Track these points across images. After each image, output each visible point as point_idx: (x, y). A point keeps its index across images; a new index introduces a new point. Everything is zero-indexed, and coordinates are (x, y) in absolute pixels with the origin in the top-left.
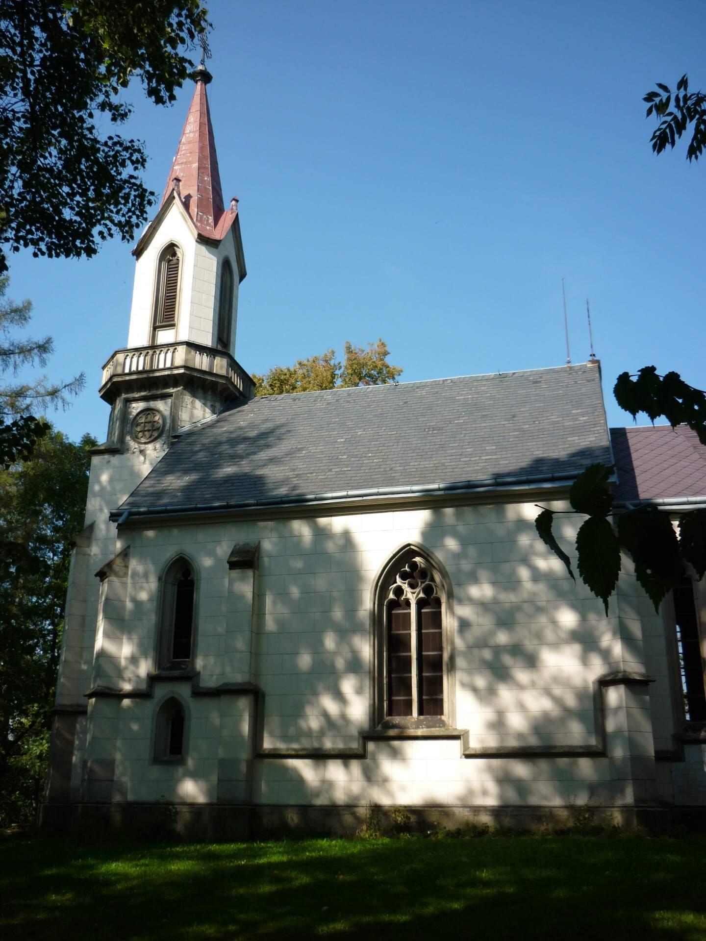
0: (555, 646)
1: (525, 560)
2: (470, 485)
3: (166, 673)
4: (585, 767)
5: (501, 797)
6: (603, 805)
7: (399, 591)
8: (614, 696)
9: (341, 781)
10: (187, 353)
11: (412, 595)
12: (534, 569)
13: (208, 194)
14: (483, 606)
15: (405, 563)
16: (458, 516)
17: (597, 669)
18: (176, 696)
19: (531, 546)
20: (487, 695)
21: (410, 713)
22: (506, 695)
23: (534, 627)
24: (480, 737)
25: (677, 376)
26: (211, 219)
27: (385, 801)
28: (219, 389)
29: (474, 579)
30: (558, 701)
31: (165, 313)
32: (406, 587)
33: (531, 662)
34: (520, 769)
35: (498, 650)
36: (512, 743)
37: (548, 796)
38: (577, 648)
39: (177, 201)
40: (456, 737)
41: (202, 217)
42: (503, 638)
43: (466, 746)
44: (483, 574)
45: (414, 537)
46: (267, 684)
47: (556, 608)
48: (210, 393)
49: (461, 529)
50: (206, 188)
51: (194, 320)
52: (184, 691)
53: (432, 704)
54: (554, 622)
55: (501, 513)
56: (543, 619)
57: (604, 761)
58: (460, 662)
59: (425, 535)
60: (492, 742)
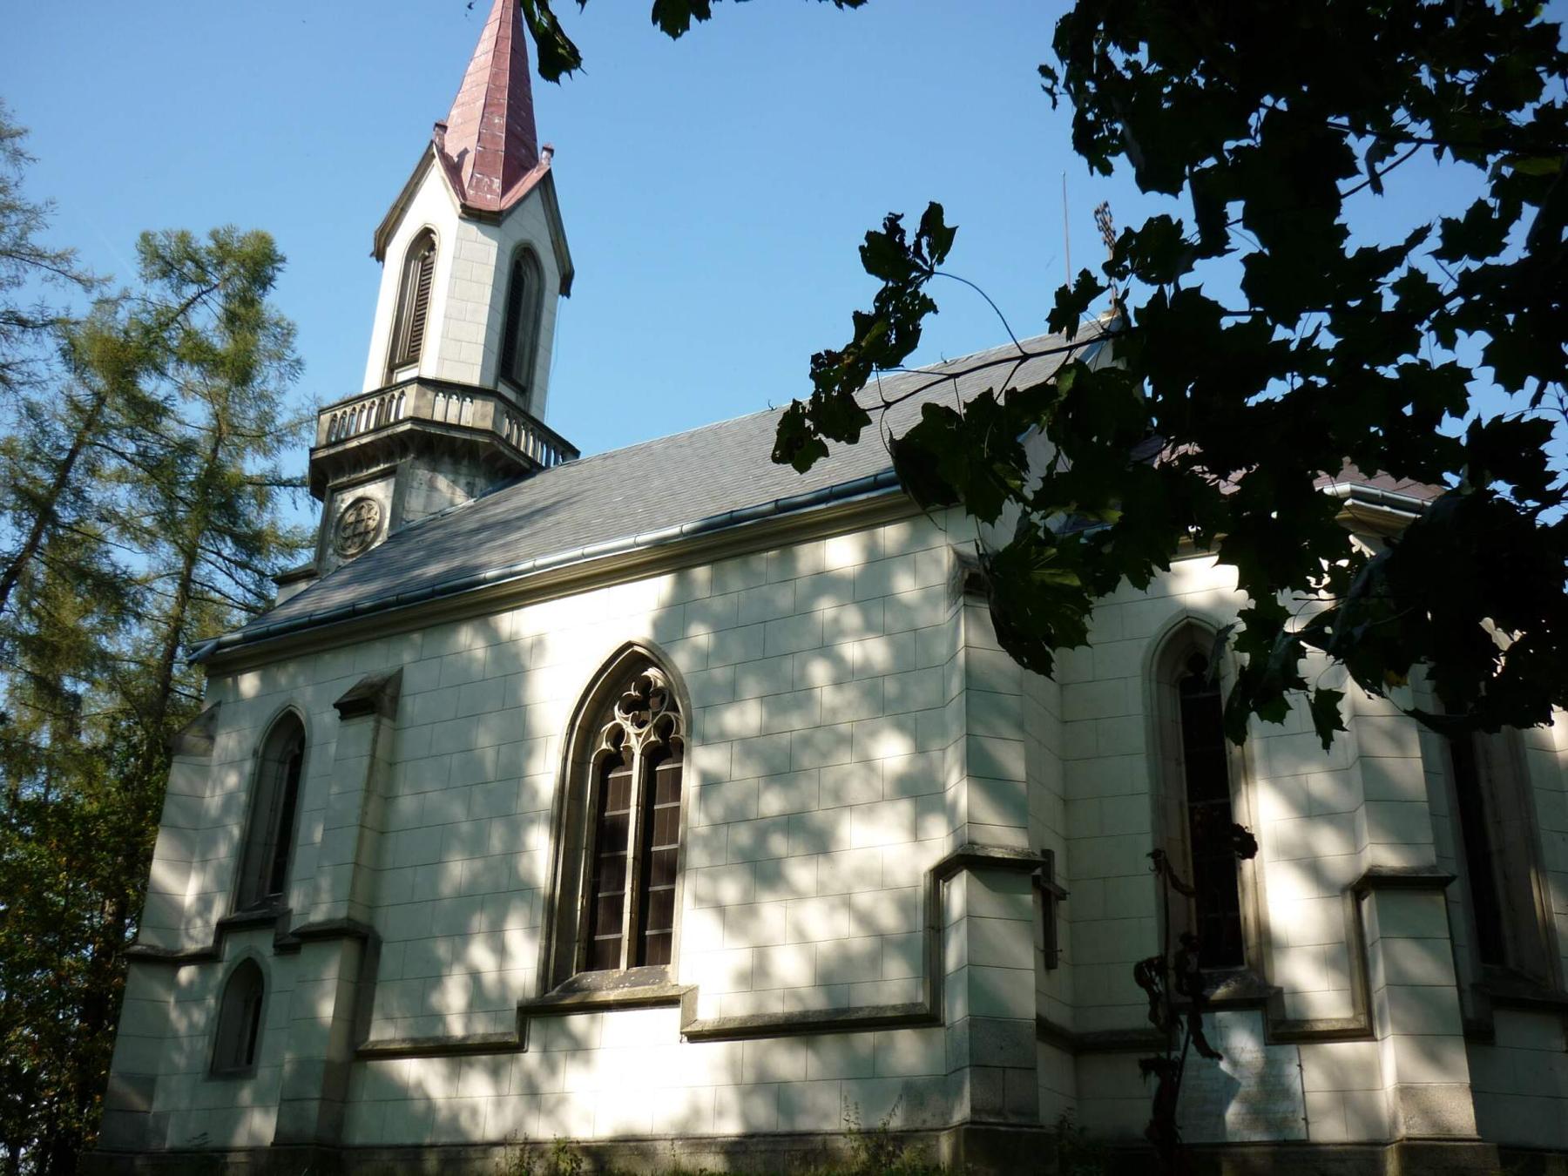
0: (869, 809)
1: (825, 648)
2: (733, 519)
3: (245, 916)
4: (908, 1051)
5: (745, 1117)
6: (928, 1125)
7: (618, 735)
8: (957, 893)
9: (479, 1102)
10: (419, 396)
11: (635, 741)
12: (837, 661)
13: (497, 144)
14: (747, 747)
15: (624, 679)
16: (716, 583)
17: (939, 844)
18: (258, 959)
19: (836, 621)
20: (738, 918)
21: (617, 966)
22: (773, 913)
23: (830, 777)
24: (720, 1001)
25: (1507, 390)
26: (497, 184)
27: (541, 1129)
28: (482, 455)
29: (733, 695)
30: (865, 920)
31: (406, 346)
32: (630, 729)
33: (820, 844)
34: (788, 1061)
35: (764, 828)
36: (778, 1007)
37: (833, 1114)
38: (904, 808)
39: (437, 161)
40: (671, 1002)
41: (479, 181)
42: (772, 803)
43: (687, 1019)
44: (751, 686)
45: (640, 631)
46: (390, 925)
47: (873, 734)
48: (465, 462)
49: (718, 605)
50: (494, 136)
51: (458, 343)
52: (263, 945)
53: (653, 946)
54: (867, 762)
55: (789, 561)
56: (846, 761)
57: (938, 1034)
58: (696, 857)
59: (658, 625)
60: (738, 1007)
